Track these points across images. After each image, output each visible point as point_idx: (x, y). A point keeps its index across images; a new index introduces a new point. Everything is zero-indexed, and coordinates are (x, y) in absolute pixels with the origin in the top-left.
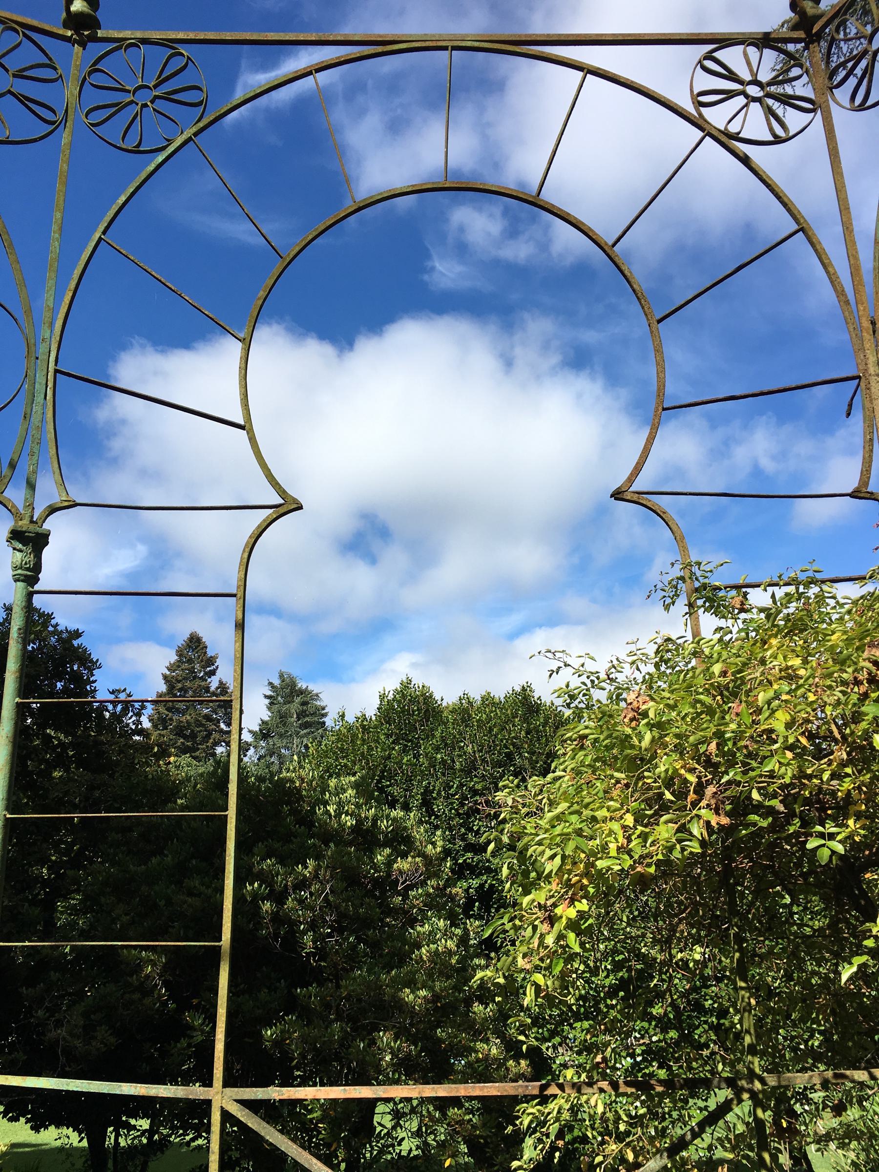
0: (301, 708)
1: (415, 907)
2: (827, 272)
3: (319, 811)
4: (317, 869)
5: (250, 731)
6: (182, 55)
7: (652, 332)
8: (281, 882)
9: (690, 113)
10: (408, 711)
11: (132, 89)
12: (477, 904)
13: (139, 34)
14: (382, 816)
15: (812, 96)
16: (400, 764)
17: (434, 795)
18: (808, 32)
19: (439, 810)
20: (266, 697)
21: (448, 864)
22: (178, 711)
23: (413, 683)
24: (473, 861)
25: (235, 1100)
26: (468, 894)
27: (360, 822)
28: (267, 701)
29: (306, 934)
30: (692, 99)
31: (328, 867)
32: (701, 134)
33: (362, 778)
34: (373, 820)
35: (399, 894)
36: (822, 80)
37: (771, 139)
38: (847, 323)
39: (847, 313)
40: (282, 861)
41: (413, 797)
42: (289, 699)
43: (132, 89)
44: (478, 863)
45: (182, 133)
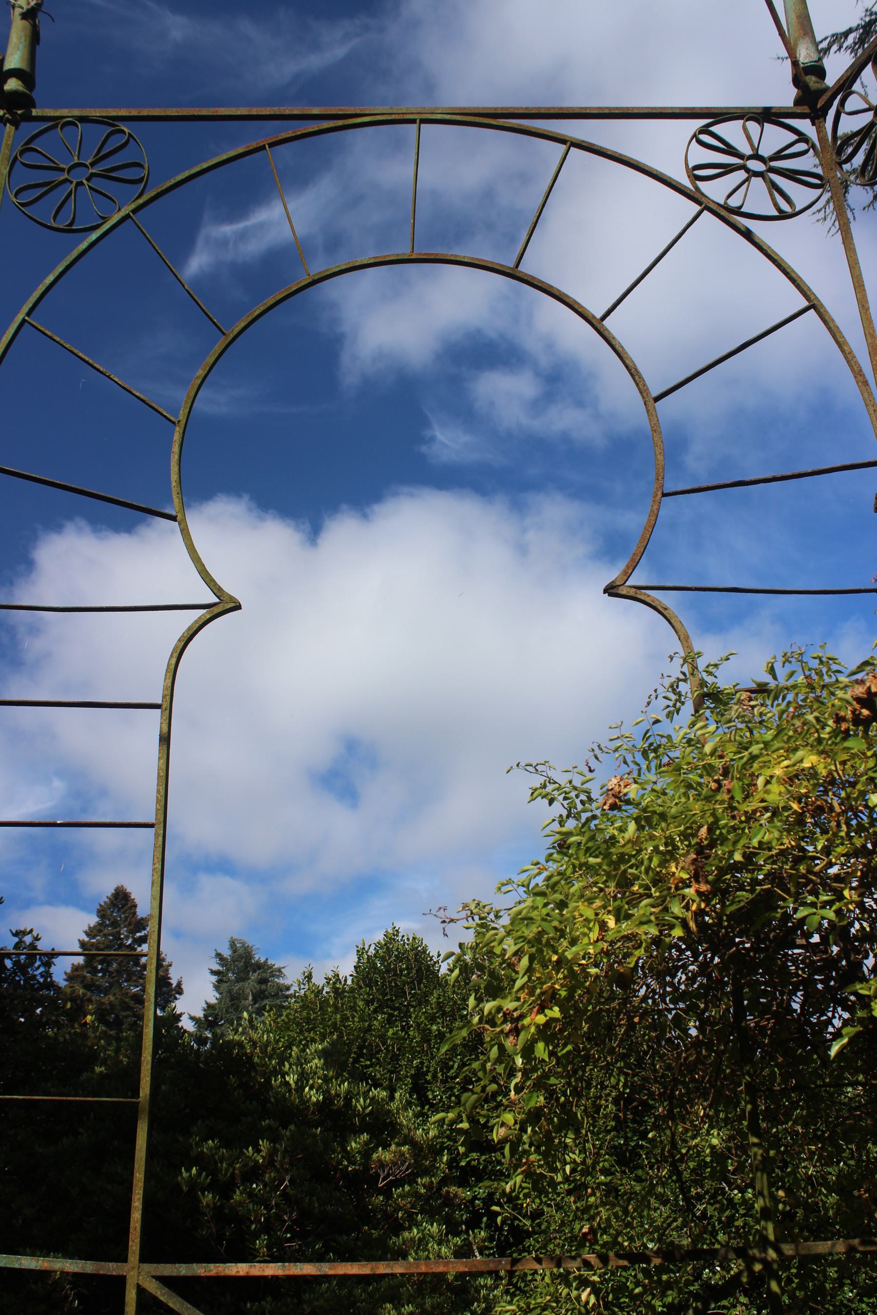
0: (258, 987)
1: (400, 1209)
2: (843, 351)
3: (276, 1082)
4: (272, 1153)
5: (192, 1018)
6: (123, 132)
7: (648, 411)
8: (227, 1170)
9: (685, 187)
10: (395, 969)
11: (66, 167)
12: (485, 1219)
13: (77, 112)
14: (358, 1093)
15: (819, 171)
16: (383, 1038)
17: (429, 1078)
18: (813, 106)
19: (435, 1097)
20: (213, 972)
21: (445, 1158)
22: (99, 989)
23: (400, 935)
24: (479, 1163)
25: (154, 1277)
26: (474, 1207)
27: (329, 1098)
28: (214, 978)
29: (258, 1237)
30: (687, 172)
31: (286, 1151)
32: (698, 208)
33: (333, 1044)
34: (345, 1098)
35: (380, 1192)
36: (831, 156)
37: (776, 213)
38: (867, 406)
39: (866, 394)
40: (227, 1143)
41: (401, 1079)
42: (242, 978)
43: (66, 167)
44: (485, 1167)
45: (119, 210)
